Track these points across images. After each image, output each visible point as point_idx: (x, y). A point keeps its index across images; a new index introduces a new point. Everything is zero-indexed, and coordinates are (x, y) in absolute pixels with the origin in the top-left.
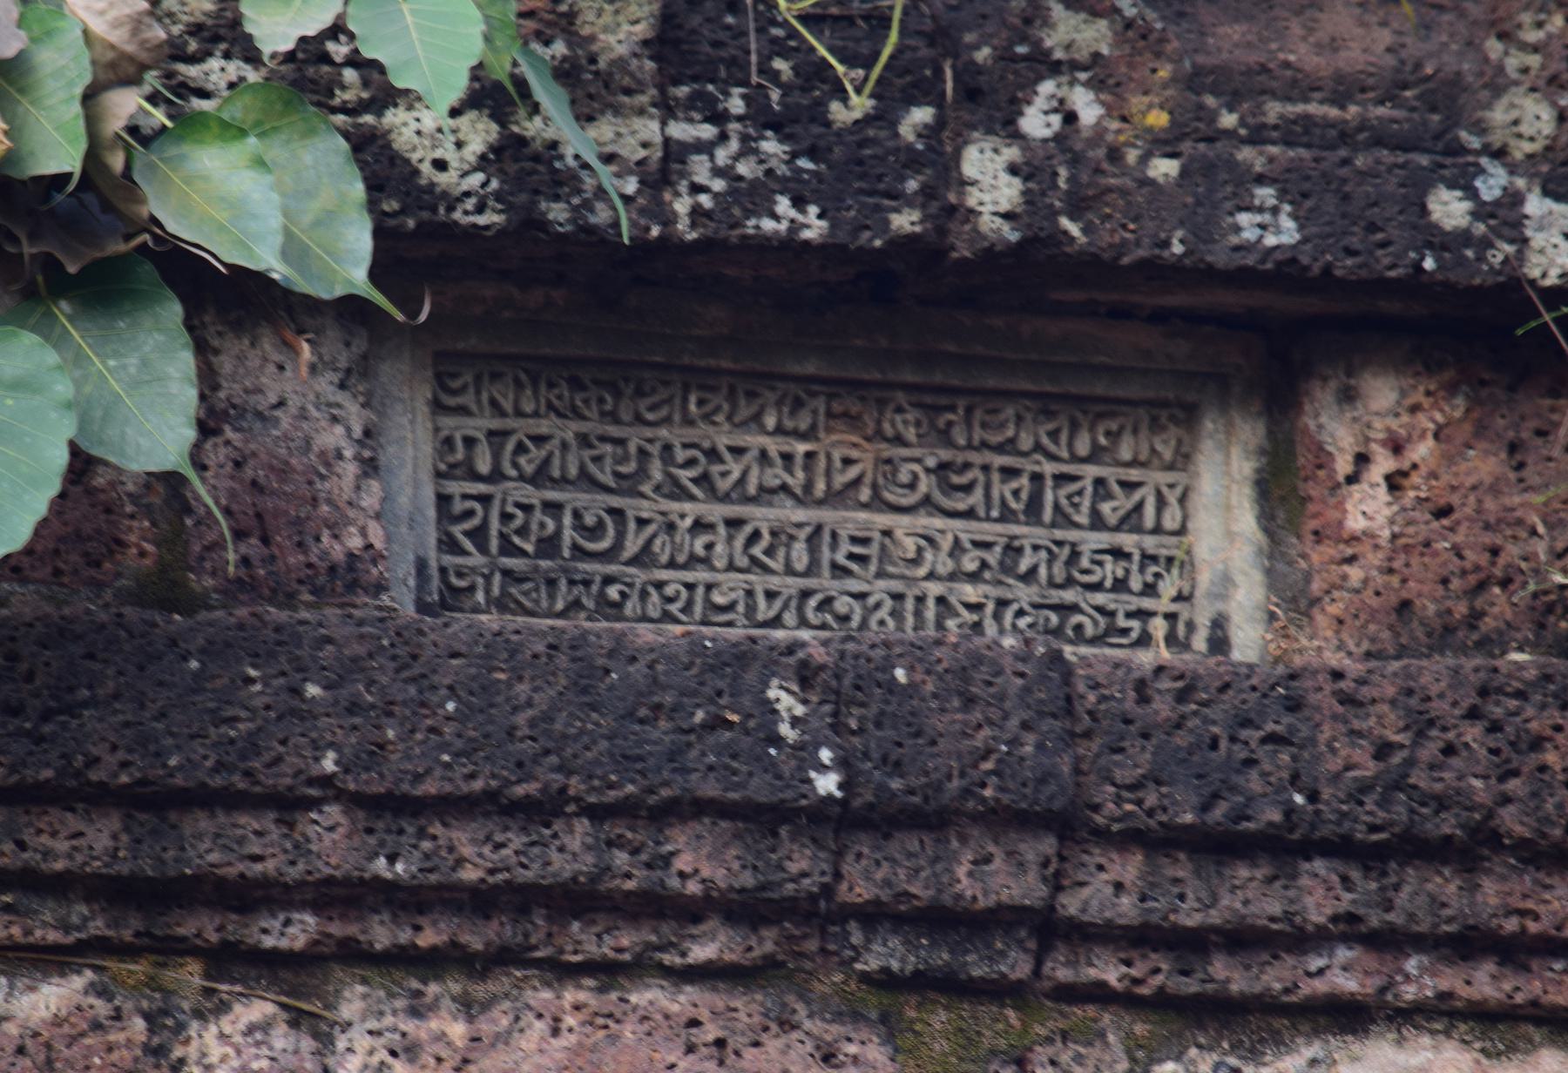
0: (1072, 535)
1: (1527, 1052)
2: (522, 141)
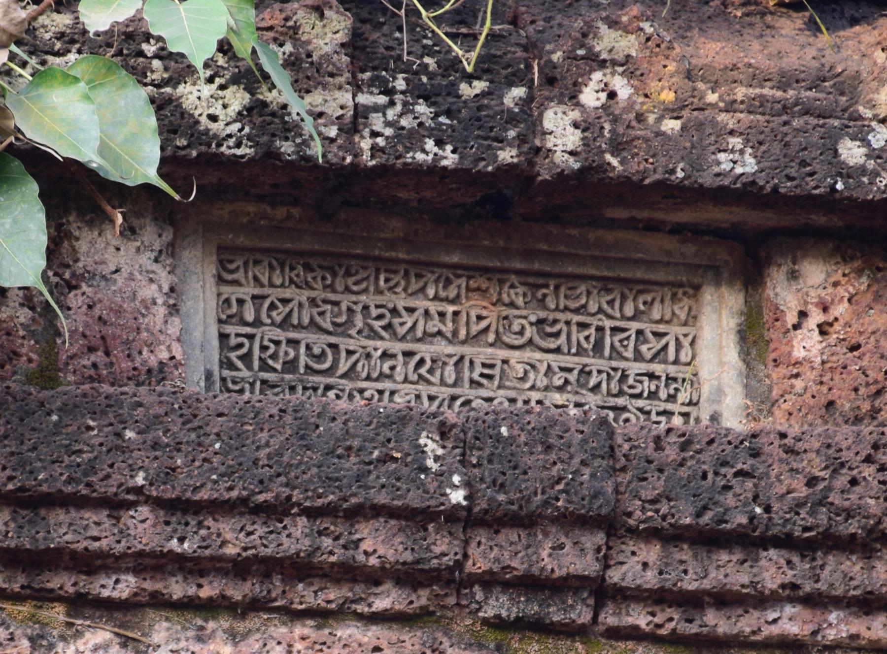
0: (623, 364)
2: (264, 104)
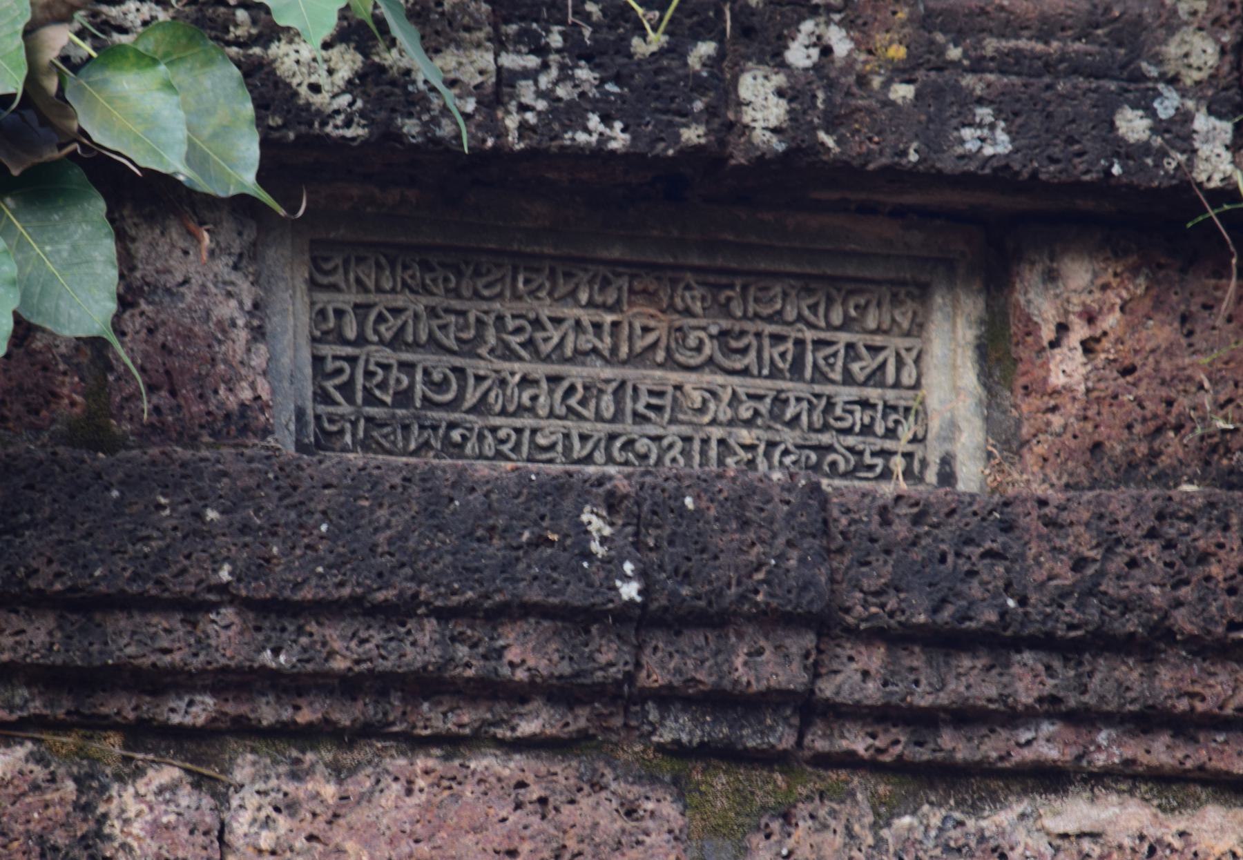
0: (828, 389)
1: (1195, 808)
2: (382, 69)
